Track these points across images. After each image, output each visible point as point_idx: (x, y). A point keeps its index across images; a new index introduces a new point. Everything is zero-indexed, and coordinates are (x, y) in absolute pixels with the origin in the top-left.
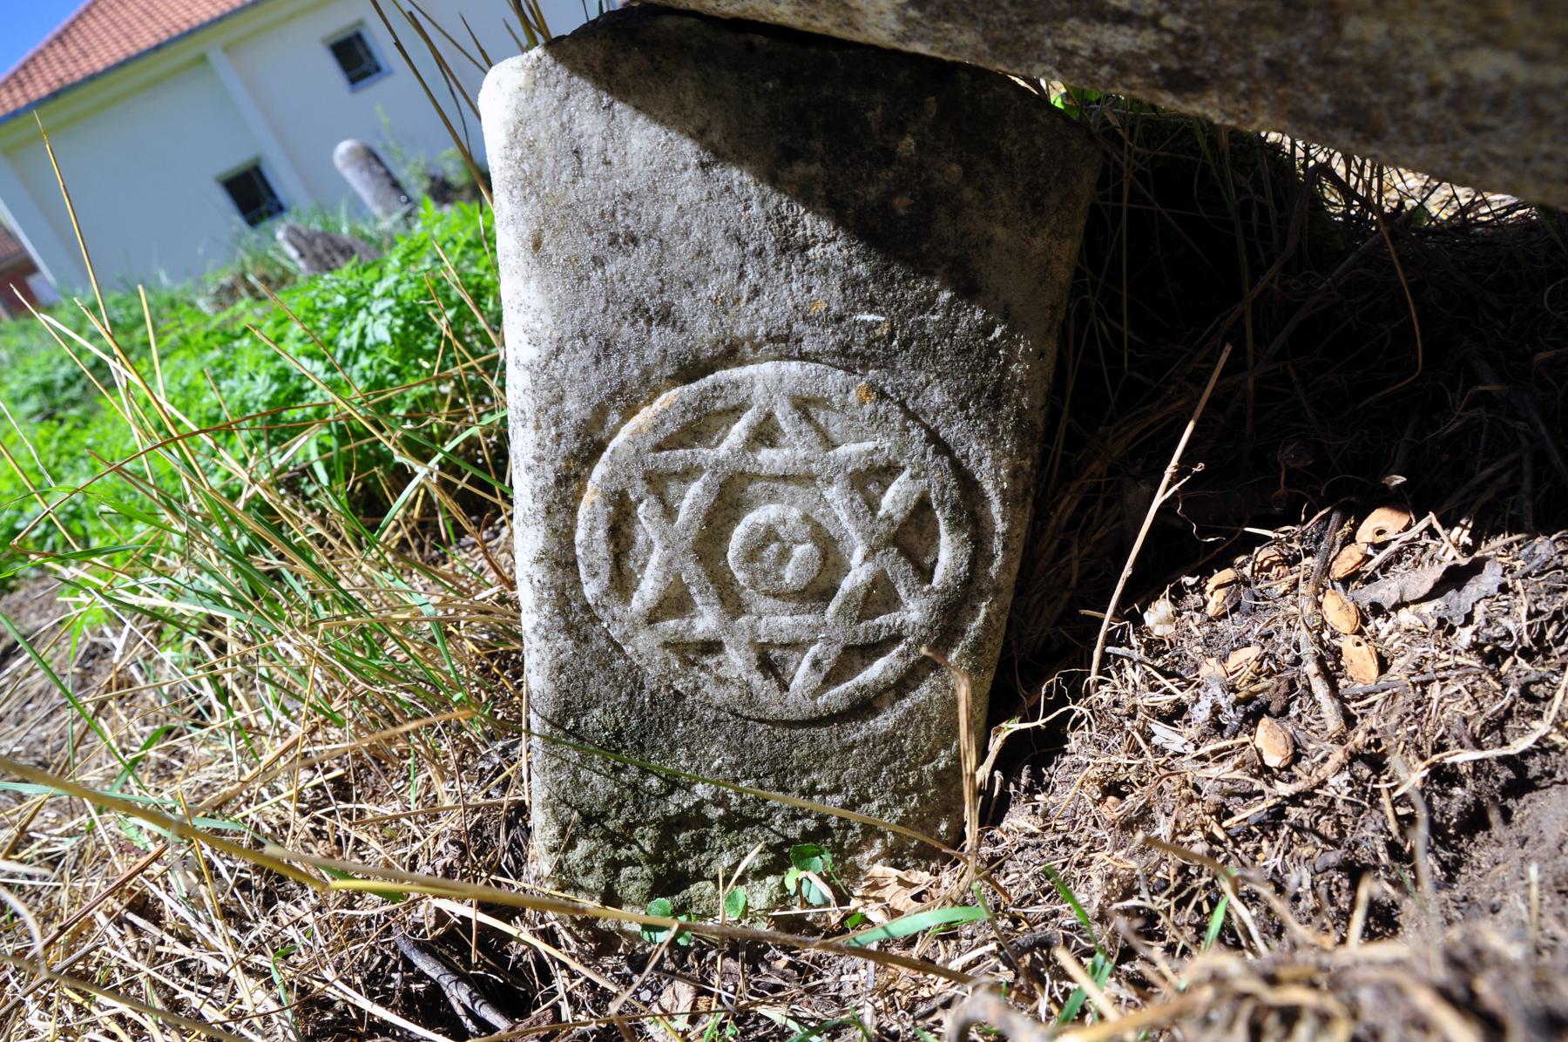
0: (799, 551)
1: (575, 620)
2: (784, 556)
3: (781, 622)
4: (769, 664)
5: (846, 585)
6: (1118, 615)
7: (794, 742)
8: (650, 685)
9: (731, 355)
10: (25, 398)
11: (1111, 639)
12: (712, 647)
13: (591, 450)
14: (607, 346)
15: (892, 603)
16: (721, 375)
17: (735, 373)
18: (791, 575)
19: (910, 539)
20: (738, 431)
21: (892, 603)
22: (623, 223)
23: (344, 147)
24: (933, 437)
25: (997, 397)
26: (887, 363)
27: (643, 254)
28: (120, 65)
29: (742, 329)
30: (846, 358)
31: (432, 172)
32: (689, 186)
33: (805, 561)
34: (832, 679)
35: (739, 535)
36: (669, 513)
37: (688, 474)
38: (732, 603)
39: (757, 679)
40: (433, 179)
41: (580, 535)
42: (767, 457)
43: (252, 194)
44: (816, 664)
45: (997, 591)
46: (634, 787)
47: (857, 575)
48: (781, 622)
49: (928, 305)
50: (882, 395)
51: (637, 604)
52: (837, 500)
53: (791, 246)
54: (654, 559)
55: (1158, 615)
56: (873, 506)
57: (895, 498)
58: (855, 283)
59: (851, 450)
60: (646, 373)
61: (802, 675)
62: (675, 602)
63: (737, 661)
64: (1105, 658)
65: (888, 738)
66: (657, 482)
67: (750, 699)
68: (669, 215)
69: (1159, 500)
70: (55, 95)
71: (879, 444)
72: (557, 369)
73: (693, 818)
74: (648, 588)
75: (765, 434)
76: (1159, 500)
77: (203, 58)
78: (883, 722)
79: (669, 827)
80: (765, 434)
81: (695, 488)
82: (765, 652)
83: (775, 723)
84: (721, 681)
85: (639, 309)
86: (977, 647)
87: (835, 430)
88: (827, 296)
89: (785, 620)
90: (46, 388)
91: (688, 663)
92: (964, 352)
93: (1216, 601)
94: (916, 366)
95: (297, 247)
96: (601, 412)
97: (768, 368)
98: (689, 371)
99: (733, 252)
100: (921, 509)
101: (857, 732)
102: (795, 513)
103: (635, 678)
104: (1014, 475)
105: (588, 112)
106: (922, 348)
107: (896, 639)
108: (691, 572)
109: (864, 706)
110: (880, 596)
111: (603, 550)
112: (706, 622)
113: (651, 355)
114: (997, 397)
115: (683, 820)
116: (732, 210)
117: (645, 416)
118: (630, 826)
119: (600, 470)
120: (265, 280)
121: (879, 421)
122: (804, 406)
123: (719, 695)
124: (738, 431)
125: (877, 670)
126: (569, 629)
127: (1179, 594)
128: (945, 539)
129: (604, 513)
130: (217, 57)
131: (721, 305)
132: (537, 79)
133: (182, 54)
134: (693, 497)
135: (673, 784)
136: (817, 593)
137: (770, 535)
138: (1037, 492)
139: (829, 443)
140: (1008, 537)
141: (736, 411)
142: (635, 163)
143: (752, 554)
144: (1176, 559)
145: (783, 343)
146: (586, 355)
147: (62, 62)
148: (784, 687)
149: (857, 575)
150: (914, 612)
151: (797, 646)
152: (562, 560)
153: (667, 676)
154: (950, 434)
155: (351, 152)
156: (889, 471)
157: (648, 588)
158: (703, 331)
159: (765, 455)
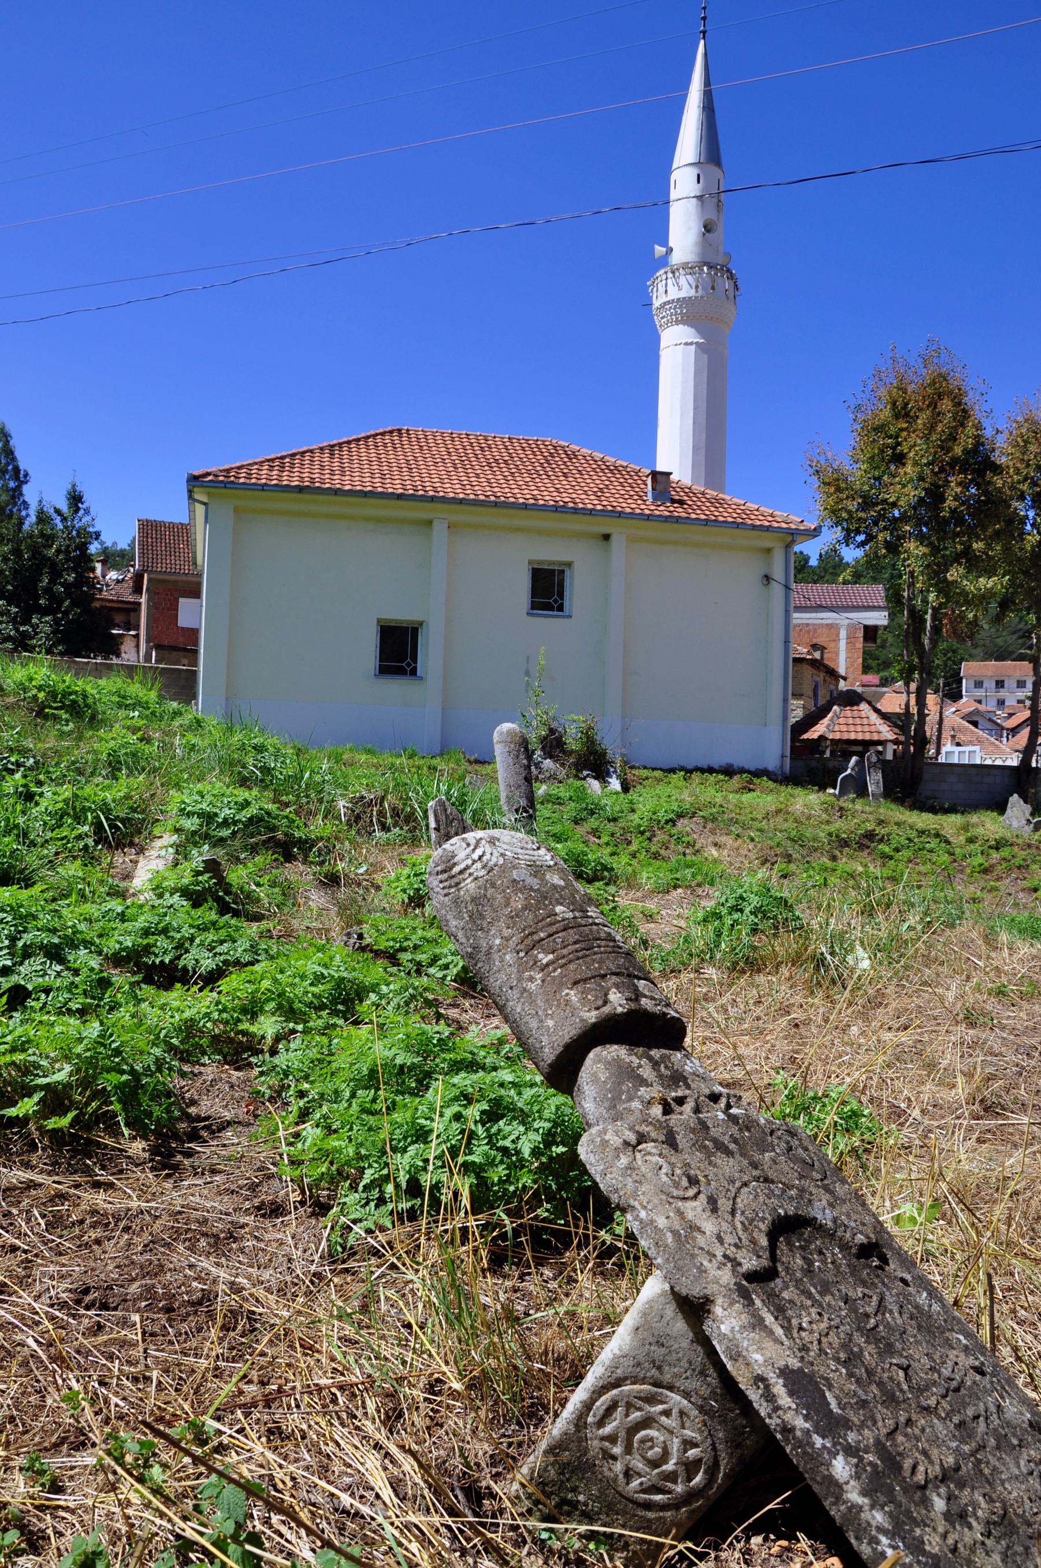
0: (657, 1449)
1: (580, 1421)
2: (651, 1448)
3: (639, 1465)
4: (629, 1474)
5: (664, 1467)
6: (742, 1531)
7: (620, 1502)
8: (589, 1456)
9: (671, 1388)
10: (189, 815)
11: (736, 1537)
12: (614, 1458)
13: (617, 1384)
14: (639, 1364)
15: (675, 1481)
16: (665, 1391)
17: (669, 1393)
18: (650, 1454)
19: (690, 1468)
20: (660, 1408)
21: (675, 1482)
22: (662, 1340)
23: (507, 726)
24: (713, 1444)
25: (738, 1446)
26: (712, 1418)
27: (663, 1350)
28: (365, 494)
29: (677, 1384)
30: (701, 1409)
31: (554, 725)
32: (685, 1343)
33: (656, 1453)
34: (644, 1491)
35: (643, 1433)
36: (627, 1415)
37: (639, 1409)
38: (628, 1450)
39: (621, 1476)
40: (552, 731)
41: (598, 1404)
42: (664, 1419)
43: (398, 649)
44: (641, 1484)
45: (708, 1499)
46: (562, 1482)
47: (669, 1466)
48: (639, 1465)
49: (732, 1411)
50: (705, 1425)
51: (601, 1432)
52: (675, 1444)
53: (703, 1373)
54: (614, 1424)
55: (756, 1540)
56: (685, 1451)
57: (692, 1453)
58: (715, 1393)
59: (688, 1433)
60: (645, 1378)
61: (635, 1484)
62: (612, 1439)
63: (618, 1467)
64: (731, 1543)
65: (649, 1521)
66: (629, 1406)
67: (615, 1480)
68: (676, 1346)
69: (770, 1507)
70: (300, 489)
71: (696, 1436)
72: (622, 1360)
73: (574, 1505)
74: (607, 1430)
75: (667, 1413)
76: (770, 1507)
77: (430, 523)
78: (651, 1515)
79: (564, 1502)
80: (667, 1413)
81: (638, 1414)
82: (631, 1471)
83: (618, 1492)
84: (610, 1469)
85: (654, 1362)
86: (692, 1512)
87: (687, 1425)
88: (705, 1391)
89: (640, 1465)
90: (208, 818)
91: (604, 1458)
92: (735, 1429)
93: (775, 1550)
94: (719, 1423)
95: (437, 821)
96: (626, 1379)
97: (678, 1398)
98: (657, 1384)
99: (687, 1365)
100: (698, 1462)
101: (641, 1513)
102: (662, 1439)
103: (586, 1450)
104: (731, 1470)
105: (670, 1310)
106: (724, 1421)
107: (669, 1492)
108: (622, 1434)
109: (648, 1506)
110: (672, 1477)
111: (601, 1412)
112: (617, 1450)
113: (648, 1374)
114: (738, 1446)
115: (569, 1503)
116: (693, 1355)
117: (636, 1387)
118: (552, 1493)
119: (615, 1392)
120: (396, 813)
121: (701, 1431)
122: (682, 1413)
123: (607, 1473)
124: (660, 1408)
125: (658, 1497)
126: (576, 1425)
127: (766, 1539)
128: (701, 1474)
129: (609, 1403)
130: (440, 528)
131: (676, 1376)
132: (663, 1293)
133: (415, 511)
134: (636, 1416)
135: (574, 1490)
136: (654, 1464)
137: (651, 1439)
138: (734, 1478)
139: (683, 1427)
140: (720, 1486)
141: (662, 1403)
142: (675, 1329)
143: (643, 1441)
144: (766, 1527)
145: (686, 1395)
146: (631, 1363)
147: (322, 468)
148: (628, 1484)
149: (669, 1466)
150: (679, 1488)
151: (640, 1475)
152: (587, 1406)
153: (595, 1457)
154: (720, 1447)
155: (509, 733)
156: (696, 1446)
157: (607, 1430)
158: (667, 1378)
159: (663, 1418)
